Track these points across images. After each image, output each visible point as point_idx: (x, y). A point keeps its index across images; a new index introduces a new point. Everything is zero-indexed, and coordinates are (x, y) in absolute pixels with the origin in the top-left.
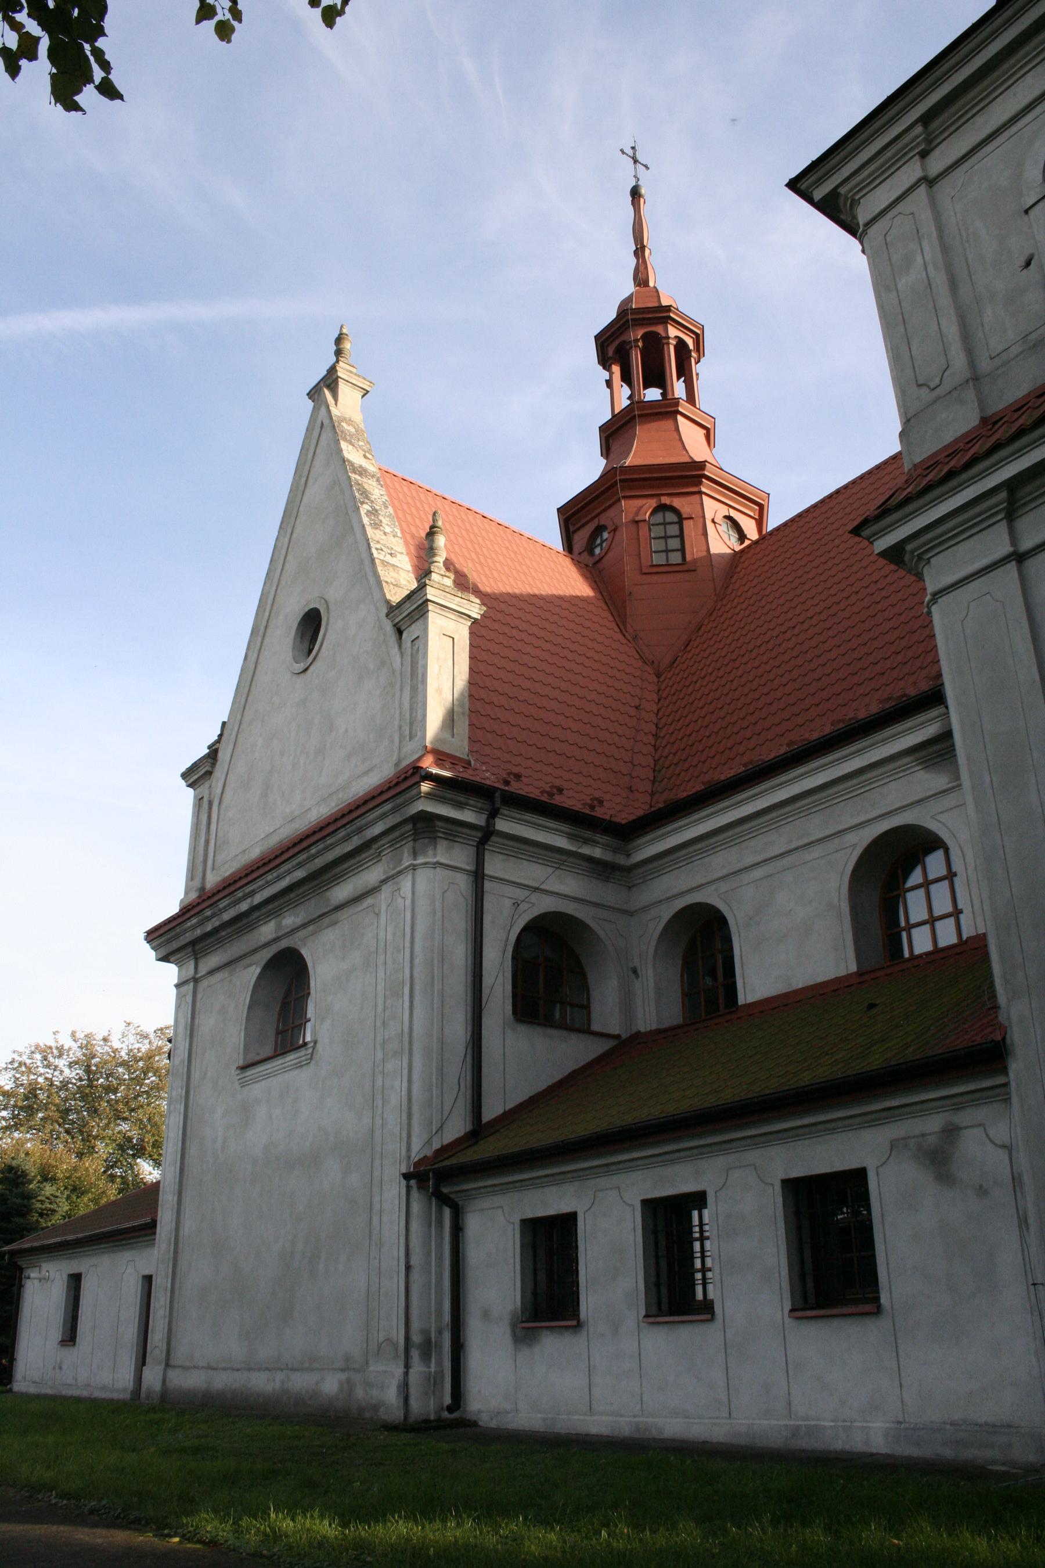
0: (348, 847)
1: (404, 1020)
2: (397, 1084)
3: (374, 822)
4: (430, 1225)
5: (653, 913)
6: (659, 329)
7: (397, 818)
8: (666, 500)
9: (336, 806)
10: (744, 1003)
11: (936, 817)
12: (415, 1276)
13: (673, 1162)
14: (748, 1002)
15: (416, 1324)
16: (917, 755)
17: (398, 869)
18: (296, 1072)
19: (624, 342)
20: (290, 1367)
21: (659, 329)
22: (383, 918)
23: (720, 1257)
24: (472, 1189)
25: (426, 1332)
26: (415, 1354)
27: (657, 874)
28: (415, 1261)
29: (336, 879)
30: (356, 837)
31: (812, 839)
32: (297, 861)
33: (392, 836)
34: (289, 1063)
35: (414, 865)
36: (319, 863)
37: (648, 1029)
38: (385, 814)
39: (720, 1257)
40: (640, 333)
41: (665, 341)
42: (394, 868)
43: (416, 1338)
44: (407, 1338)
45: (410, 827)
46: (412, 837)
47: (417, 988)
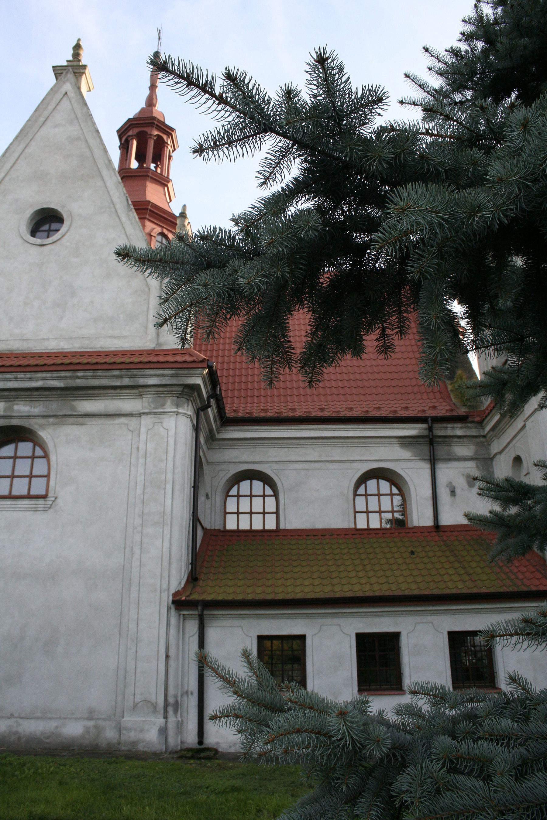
0: (118, 383)
1: (166, 504)
2: (158, 543)
3: (151, 376)
4: (179, 632)
5: (224, 467)
6: (148, 130)
7: (175, 381)
8: (165, 231)
9: (79, 348)
10: (284, 528)
11: (405, 470)
12: (172, 663)
13: (380, 616)
14: (287, 528)
15: (171, 692)
16: (400, 440)
17: (155, 411)
18: (28, 513)
19: (146, 132)
20: (16, 715)
21: (148, 130)
22: (143, 437)
23: (410, 664)
24: (218, 614)
25: (176, 696)
26: (170, 710)
27: (228, 447)
28: (172, 653)
29: (87, 397)
30: (128, 379)
31: (334, 459)
32: (59, 375)
33: (161, 389)
34: (22, 506)
35: (178, 412)
36: (79, 382)
37: (213, 528)
38: (164, 375)
39: (410, 664)
40: (156, 133)
41: (166, 145)
42: (156, 408)
43: (171, 700)
44: (166, 700)
45: (181, 389)
46: (178, 395)
47: (177, 487)
